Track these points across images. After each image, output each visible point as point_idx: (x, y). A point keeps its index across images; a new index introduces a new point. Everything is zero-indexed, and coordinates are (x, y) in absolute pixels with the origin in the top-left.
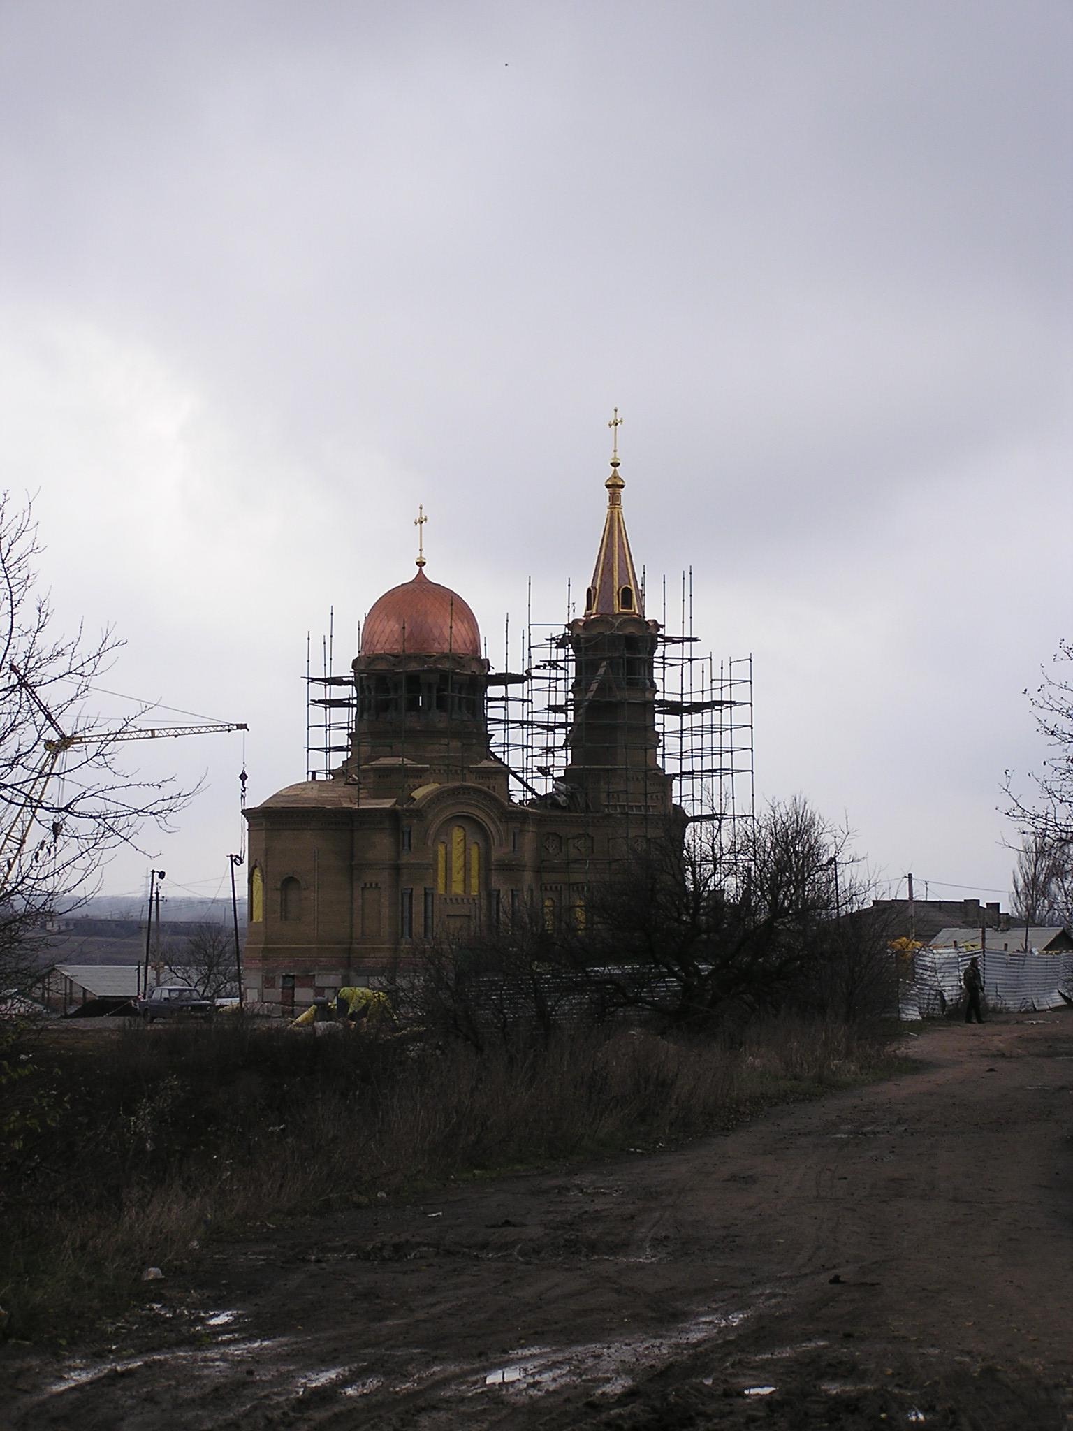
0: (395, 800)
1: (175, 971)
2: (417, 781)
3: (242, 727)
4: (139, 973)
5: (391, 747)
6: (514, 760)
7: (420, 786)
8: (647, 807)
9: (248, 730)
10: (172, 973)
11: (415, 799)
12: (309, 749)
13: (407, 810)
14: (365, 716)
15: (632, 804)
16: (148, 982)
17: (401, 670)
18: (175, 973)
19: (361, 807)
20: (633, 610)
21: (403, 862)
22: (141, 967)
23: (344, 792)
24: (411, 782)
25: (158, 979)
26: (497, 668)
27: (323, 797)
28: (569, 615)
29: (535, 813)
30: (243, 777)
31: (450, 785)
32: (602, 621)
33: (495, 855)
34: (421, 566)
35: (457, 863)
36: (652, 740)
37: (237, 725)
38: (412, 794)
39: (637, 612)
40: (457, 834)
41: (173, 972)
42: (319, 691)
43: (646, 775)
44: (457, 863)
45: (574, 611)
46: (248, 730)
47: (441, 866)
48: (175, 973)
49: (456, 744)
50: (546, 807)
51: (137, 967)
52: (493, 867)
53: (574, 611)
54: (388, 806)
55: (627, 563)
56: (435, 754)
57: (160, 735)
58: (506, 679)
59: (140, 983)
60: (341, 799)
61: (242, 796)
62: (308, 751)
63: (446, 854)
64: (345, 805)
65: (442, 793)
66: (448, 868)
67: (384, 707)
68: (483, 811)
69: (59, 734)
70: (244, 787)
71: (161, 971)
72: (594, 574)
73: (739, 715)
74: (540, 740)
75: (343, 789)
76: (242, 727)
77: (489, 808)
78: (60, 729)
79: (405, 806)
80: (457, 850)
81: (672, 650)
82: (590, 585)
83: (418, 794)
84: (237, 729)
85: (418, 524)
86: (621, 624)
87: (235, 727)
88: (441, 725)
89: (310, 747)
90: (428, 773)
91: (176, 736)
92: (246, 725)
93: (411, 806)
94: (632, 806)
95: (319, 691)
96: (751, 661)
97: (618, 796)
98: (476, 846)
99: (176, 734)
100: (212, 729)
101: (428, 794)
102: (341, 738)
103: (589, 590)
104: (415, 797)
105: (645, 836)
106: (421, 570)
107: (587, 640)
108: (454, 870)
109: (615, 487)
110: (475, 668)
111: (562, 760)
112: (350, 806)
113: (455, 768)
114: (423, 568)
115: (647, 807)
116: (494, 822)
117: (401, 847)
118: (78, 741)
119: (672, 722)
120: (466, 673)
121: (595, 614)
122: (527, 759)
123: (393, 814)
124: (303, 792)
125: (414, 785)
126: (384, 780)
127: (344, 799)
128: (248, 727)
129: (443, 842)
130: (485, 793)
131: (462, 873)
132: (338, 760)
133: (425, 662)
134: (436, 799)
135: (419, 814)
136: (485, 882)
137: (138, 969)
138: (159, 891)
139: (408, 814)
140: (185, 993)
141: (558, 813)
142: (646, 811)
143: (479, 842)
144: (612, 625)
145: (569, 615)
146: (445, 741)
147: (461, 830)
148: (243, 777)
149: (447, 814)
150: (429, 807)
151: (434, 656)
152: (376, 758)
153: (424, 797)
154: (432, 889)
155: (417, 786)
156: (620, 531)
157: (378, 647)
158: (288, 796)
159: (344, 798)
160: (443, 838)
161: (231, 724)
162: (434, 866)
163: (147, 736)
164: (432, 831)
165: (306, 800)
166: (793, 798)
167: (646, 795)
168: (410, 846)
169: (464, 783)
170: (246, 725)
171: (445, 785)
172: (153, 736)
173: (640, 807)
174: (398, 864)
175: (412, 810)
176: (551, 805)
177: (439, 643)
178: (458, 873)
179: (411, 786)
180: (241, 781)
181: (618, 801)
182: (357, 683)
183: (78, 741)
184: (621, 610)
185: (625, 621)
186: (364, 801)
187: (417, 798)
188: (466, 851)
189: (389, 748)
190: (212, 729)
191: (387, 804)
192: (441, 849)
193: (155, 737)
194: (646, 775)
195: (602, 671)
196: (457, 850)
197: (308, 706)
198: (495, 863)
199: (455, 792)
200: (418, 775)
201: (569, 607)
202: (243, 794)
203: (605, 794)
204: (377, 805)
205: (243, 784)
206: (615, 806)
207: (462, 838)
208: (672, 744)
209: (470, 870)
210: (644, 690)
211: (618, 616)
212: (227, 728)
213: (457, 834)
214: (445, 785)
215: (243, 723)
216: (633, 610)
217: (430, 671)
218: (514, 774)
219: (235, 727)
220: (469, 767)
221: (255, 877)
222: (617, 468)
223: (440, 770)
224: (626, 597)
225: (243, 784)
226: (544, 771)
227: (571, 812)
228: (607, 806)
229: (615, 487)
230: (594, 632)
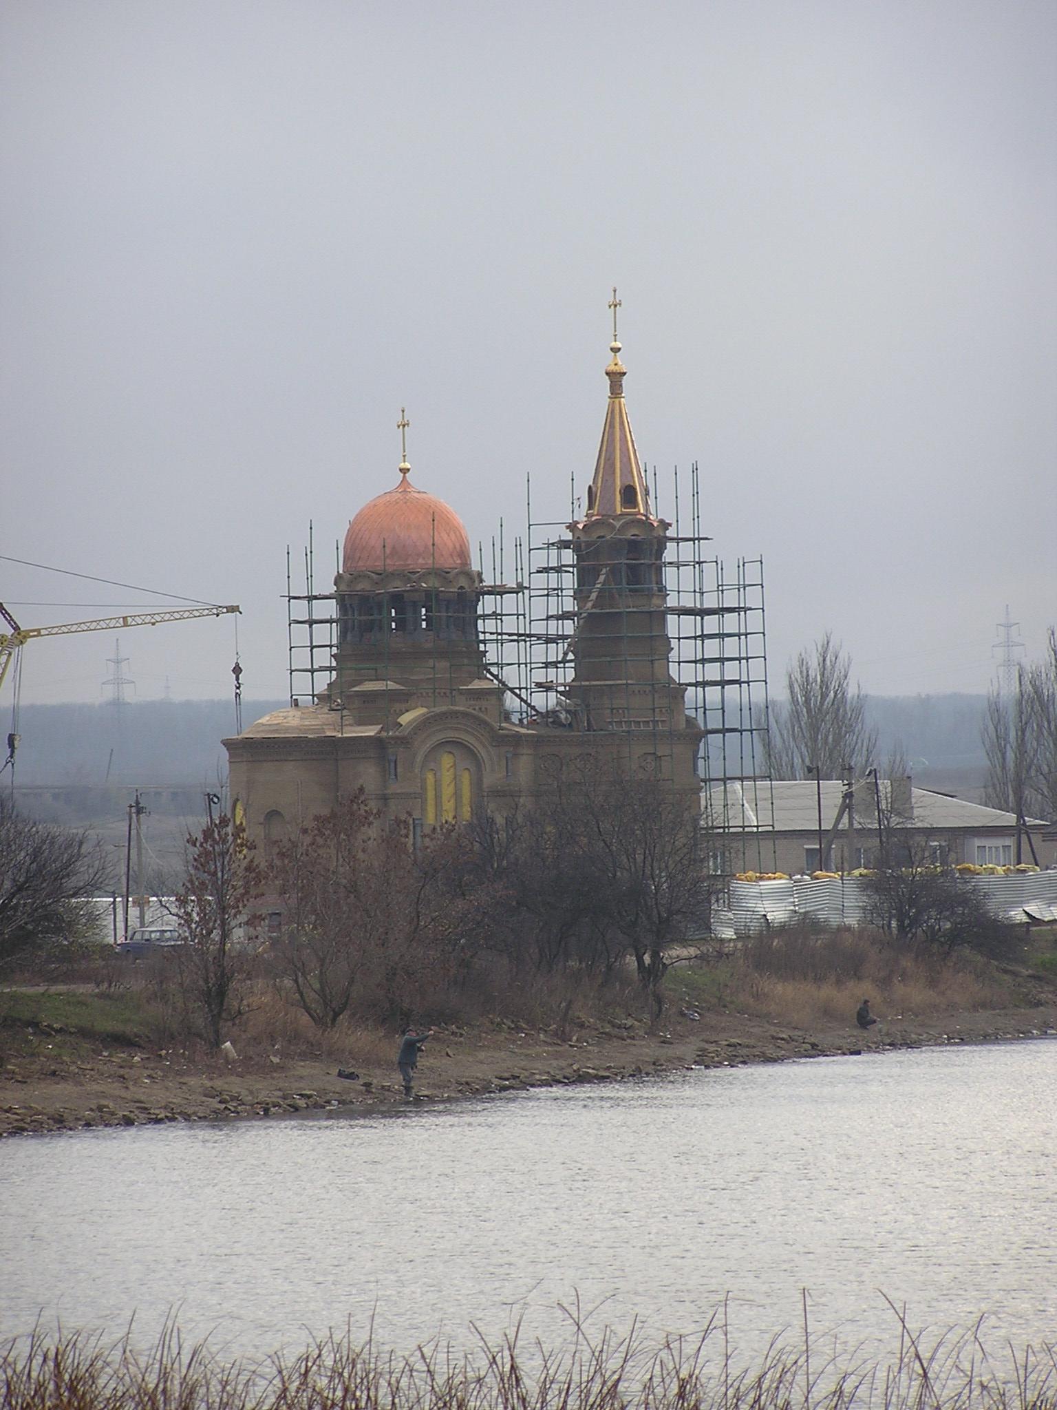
0: (381, 726)
1: (167, 905)
2: (403, 706)
3: (233, 609)
4: (114, 909)
5: (376, 669)
6: (511, 676)
7: (407, 711)
8: (655, 722)
9: (241, 613)
10: (162, 909)
11: (401, 725)
12: (292, 671)
13: (392, 738)
14: (349, 637)
15: (639, 720)
16: (129, 924)
17: (382, 591)
18: (168, 909)
19: (345, 735)
20: (637, 510)
21: (389, 791)
22: (118, 899)
23: (328, 719)
24: (397, 706)
25: (142, 917)
26: (488, 581)
27: (306, 726)
28: (573, 511)
29: (528, 735)
30: (237, 670)
31: (438, 710)
32: (603, 523)
33: (488, 781)
34: (405, 473)
35: (448, 791)
36: (659, 645)
37: (226, 607)
38: (399, 720)
39: (642, 511)
40: (447, 761)
41: (165, 907)
42: (300, 610)
43: (653, 688)
44: (448, 791)
45: (579, 506)
46: (241, 613)
47: (431, 794)
48: (168, 909)
49: (443, 664)
50: (547, 725)
51: (112, 899)
52: (485, 794)
53: (579, 506)
54: (372, 734)
55: (630, 458)
56: (422, 677)
57: (134, 623)
58: (499, 591)
59: (118, 924)
60: (324, 727)
61: (237, 693)
62: (291, 674)
63: (436, 781)
64: (329, 734)
65: (428, 718)
66: (438, 797)
67: (369, 627)
68: (473, 735)
69: (12, 626)
70: (238, 683)
71: (146, 908)
72: (596, 470)
73: (753, 621)
74: (540, 652)
75: (326, 716)
76: (233, 609)
77: (479, 732)
78: (13, 620)
79: (390, 734)
80: (447, 777)
81: (686, 551)
82: (591, 483)
83: (405, 719)
84: (227, 612)
85: (401, 427)
86: (623, 526)
87: (225, 610)
88: (429, 645)
89: (293, 668)
90: (415, 696)
91: (153, 624)
92: (238, 606)
93: (397, 733)
94: (639, 722)
95: (300, 610)
96: (762, 563)
97: (623, 712)
98: (467, 772)
99: (153, 621)
100: (197, 614)
101: (414, 720)
102: (324, 657)
103: (590, 487)
104: (402, 723)
105: (654, 754)
106: (404, 477)
107: (589, 544)
108: (445, 798)
109: (616, 378)
110: (463, 582)
111: (568, 674)
112: (333, 735)
113: (444, 691)
114: (407, 475)
115: (655, 722)
116: (484, 746)
117: (387, 776)
118: (35, 633)
119: (688, 625)
120: (452, 590)
121: (597, 515)
122: (531, 671)
123: (377, 742)
124: (285, 721)
125: (401, 710)
126: (368, 708)
127: (328, 727)
128: (241, 610)
129: (432, 770)
130: (474, 717)
131: (453, 801)
132: (323, 681)
133: (409, 580)
134: (423, 725)
135: (404, 741)
136: (477, 809)
137: (114, 902)
138: (140, 800)
139: (393, 742)
140: (166, 934)
141: (558, 732)
142: (654, 726)
143: (469, 767)
144: (613, 527)
145: (573, 511)
146: (431, 663)
147: (451, 756)
148: (237, 670)
149: (435, 740)
150: (415, 734)
151: (418, 572)
152: (360, 682)
153: (410, 723)
154: (420, 819)
155: (404, 711)
156: (622, 423)
157: (361, 563)
158: (270, 725)
159: (322, 723)
160: (432, 765)
161: (220, 607)
162: (422, 796)
163: (118, 625)
164: (419, 758)
165: (287, 730)
166: (1050, 632)
167: (654, 710)
168: (396, 775)
169: (452, 707)
170: (238, 606)
171: (432, 709)
172: (126, 625)
173: (648, 722)
174: (385, 795)
175: (397, 738)
176: (553, 723)
177: (424, 558)
178: (449, 801)
179: (397, 711)
180: (234, 676)
181: (624, 717)
182: (341, 599)
183: (35, 633)
184: (623, 510)
185: (626, 523)
186: (349, 728)
187: (404, 724)
188: (457, 779)
189: (373, 672)
190: (197, 614)
191: (371, 731)
192: (430, 778)
193: (124, 618)
194: (653, 688)
195: (602, 578)
196: (447, 777)
197: (290, 625)
198: (487, 790)
199: (444, 716)
200: (403, 699)
201: (573, 503)
202: (238, 691)
203: (609, 711)
204: (362, 732)
205: (237, 679)
206: (621, 722)
207: (451, 764)
208: (688, 650)
209: (461, 797)
210: (650, 595)
211: (621, 517)
212: (215, 611)
213: (447, 761)
214: (432, 709)
215: (235, 605)
216: (637, 510)
217: (414, 590)
218: (512, 690)
219: (225, 610)
220: (459, 689)
221: (237, 810)
222: (617, 354)
223: (427, 693)
224: (629, 495)
225: (237, 679)
226: (546, 687)
227: (573, 731)
228: (610, 723)
229: (616, 378)
230: (594, 536)
